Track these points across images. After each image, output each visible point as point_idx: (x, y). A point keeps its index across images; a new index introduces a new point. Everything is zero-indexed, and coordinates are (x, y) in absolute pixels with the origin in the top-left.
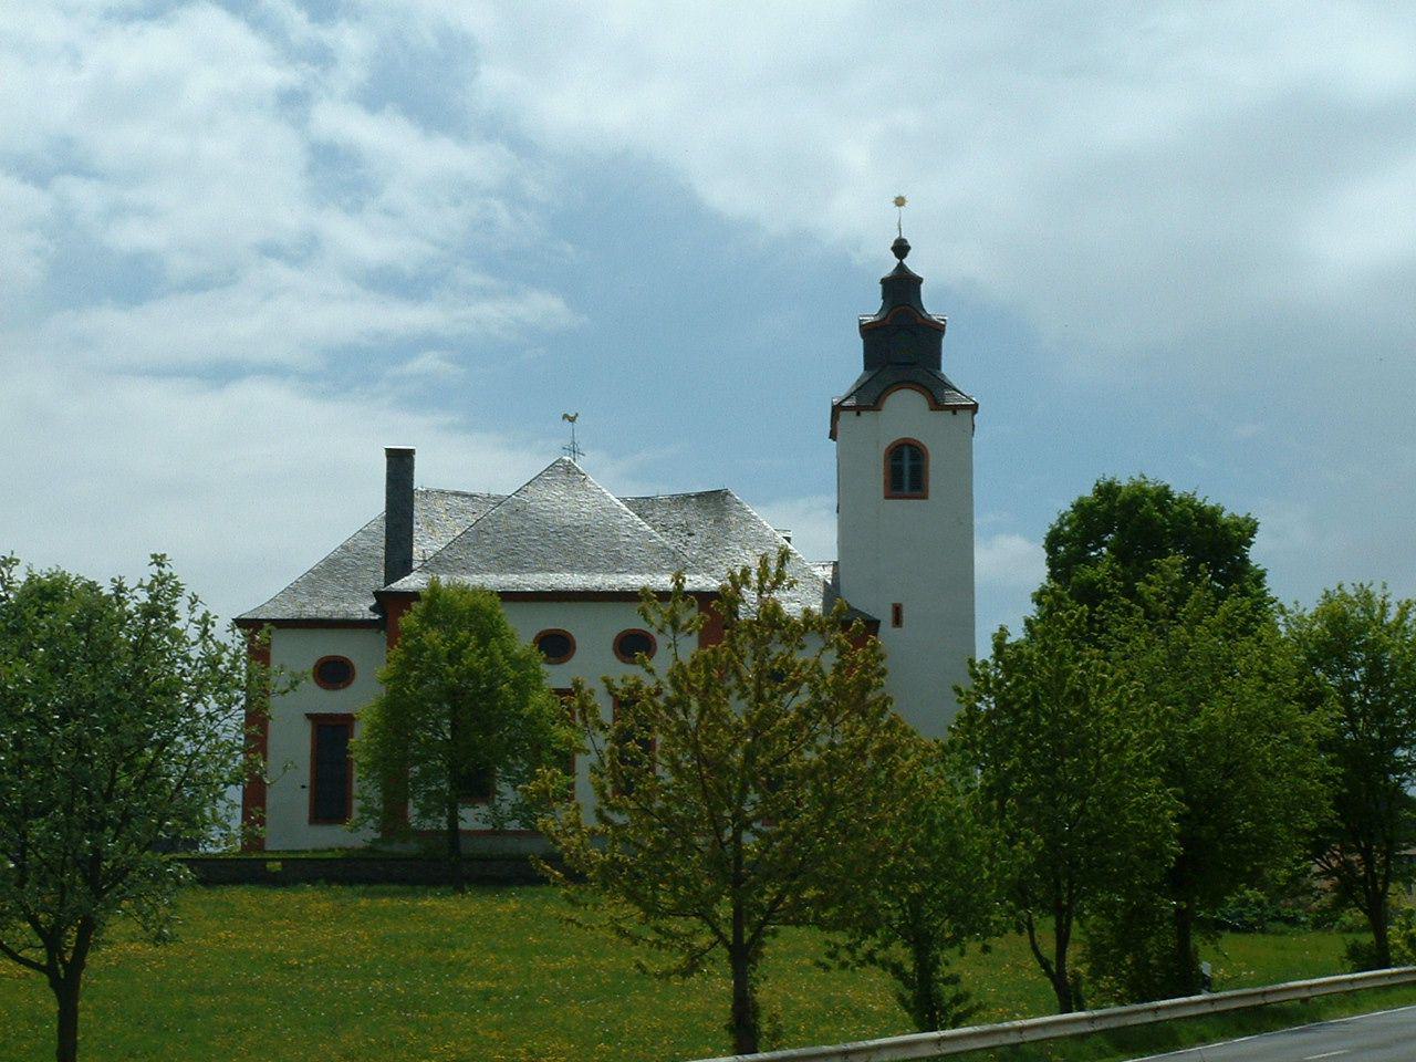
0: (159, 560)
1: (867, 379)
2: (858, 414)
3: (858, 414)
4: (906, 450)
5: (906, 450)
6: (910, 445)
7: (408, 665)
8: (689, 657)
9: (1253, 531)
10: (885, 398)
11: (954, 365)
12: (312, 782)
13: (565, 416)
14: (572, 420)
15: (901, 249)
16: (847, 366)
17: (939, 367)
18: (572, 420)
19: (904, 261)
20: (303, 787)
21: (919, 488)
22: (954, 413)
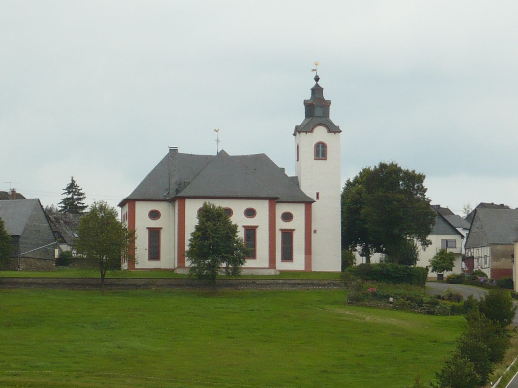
0: (14, 189)
1: (306, 123)
2: (306, 133)
3: (306, 133)
4: (321, 145)
5: (321, 145)
6: (322, 144)
7: (361, 188)
8: (11, 232)
9: (424, 177)
10: (316, 127)
11: (334, 117)
12: (148, 248)
13: (215, 130)
14: (217, 131)
15: (317, 79)
16: (300, 118)
17: (328, 117)
18: (217, 131)
19: (318, 83)
20: (146, 249)
21: (324, 157)
22: (335, 133)
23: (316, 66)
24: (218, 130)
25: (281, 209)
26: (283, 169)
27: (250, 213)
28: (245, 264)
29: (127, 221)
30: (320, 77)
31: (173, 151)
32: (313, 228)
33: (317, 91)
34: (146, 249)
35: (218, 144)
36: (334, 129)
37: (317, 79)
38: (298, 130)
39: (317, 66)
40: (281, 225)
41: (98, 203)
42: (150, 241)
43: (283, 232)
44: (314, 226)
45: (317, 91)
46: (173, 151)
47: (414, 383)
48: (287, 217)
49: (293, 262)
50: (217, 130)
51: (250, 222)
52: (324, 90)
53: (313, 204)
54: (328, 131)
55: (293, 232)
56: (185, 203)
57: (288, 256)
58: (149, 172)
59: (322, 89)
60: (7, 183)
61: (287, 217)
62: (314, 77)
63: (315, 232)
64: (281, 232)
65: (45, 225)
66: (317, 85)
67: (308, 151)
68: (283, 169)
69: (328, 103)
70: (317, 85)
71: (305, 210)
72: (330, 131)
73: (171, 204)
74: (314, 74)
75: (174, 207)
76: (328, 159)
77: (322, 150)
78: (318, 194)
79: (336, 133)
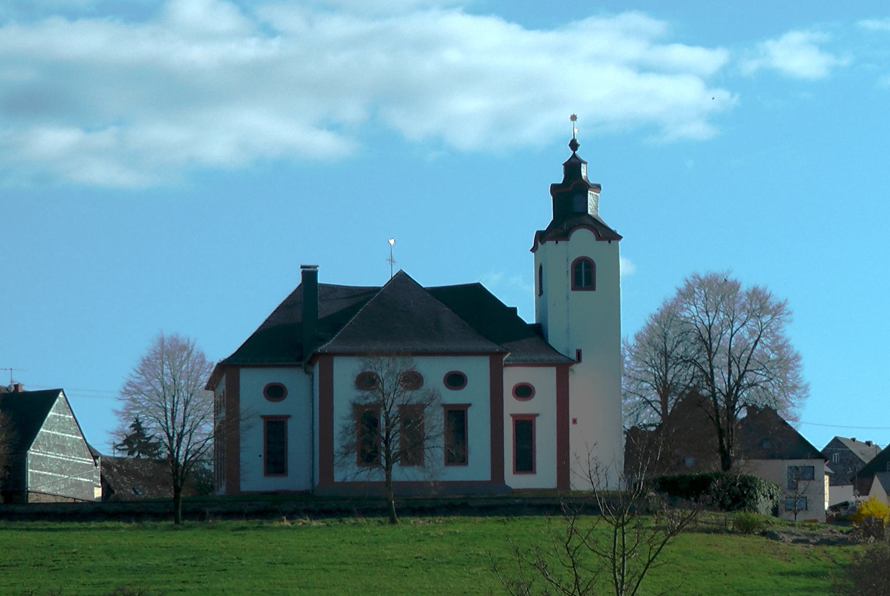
3: (610, 242)
16: (545, 217)
20: (260, 456)
25: (513, 377)
26: (514, 310)
27: (456, 380)
29: (224, 481)
32: (572, 416)
33: (573, 167)
34: (260, 456)
36: (608, 236)
38: (541, 237)
40: (512, 406)
42: (268, 442)
43: (516, 421)
44: (573, 412)
45: (573, 167)
47: (785, 310)
48: (524, 391)
49: (535, 473)
51: (453, 397)
55: (535, 420)
57: (526, 463)
60: (6, 369)
61: (524, 391)
63: (575, 421)
64: (513, 418)
65: (74, 437)
66: (574, 155)
67: (561, 277)
68: (514, 310)
70: (574, 155)
72: (599, 238)
75: (312, 375)
78: (579, 353)
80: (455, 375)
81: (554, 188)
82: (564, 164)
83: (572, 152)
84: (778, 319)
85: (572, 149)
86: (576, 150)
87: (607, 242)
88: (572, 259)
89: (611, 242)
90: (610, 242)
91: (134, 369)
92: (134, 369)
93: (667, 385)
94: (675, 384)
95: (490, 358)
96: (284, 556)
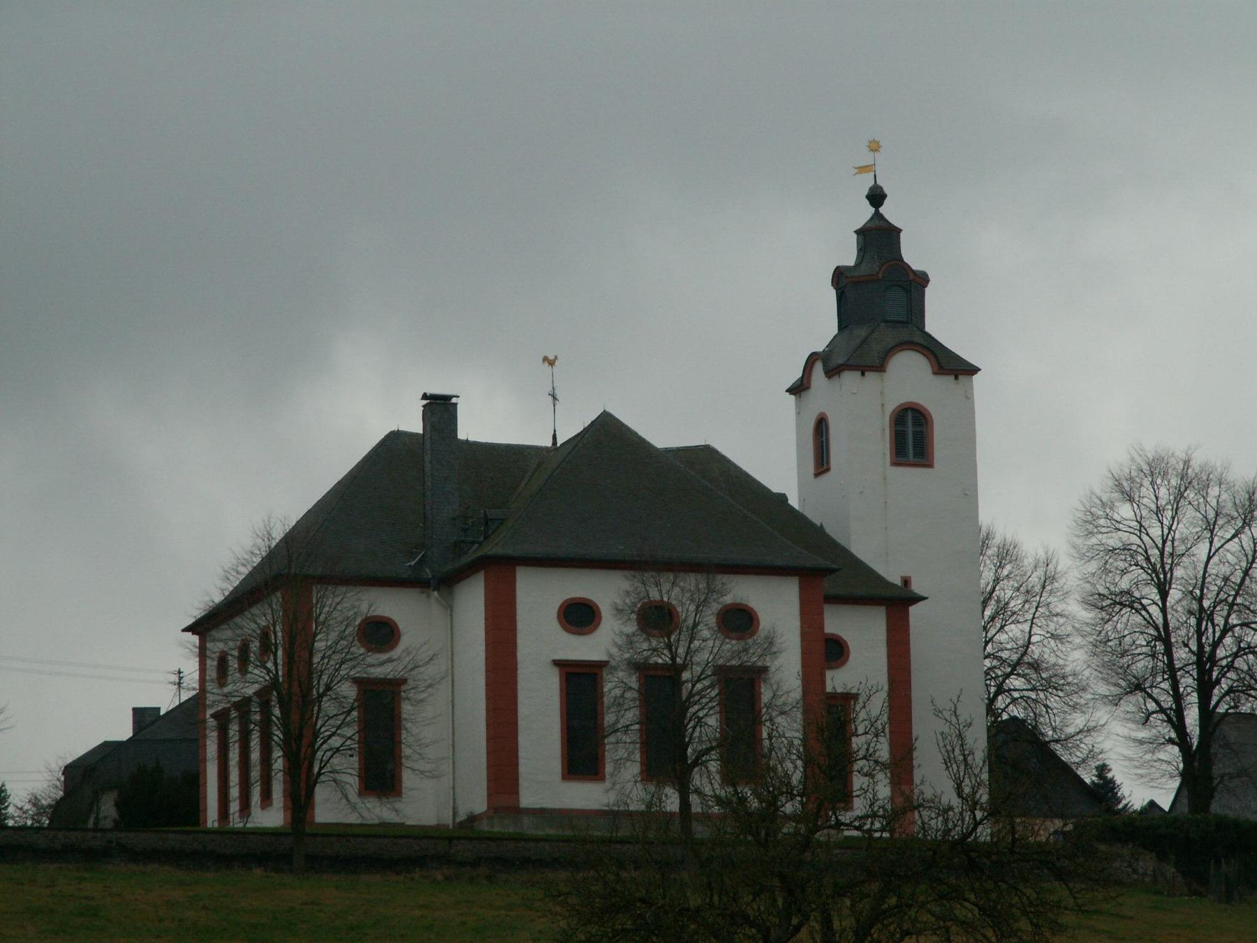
3: (863, 374)
13: (545, 359)
15: (876, 197)
19: (882, 210)
22: (956, 378)
23: (871, 153)
24: (556, 357)
28: (1032, 546)
30: (886, 190)
31: (901, 230)
35: (554, 405)
37: (876, 197)
39: (877, 154)
41: (237, 566)
46: (901, 230)
50: (551, 357)
52: (902, 235)
53: (913, 610)
54: (933, 367)
56: (515, 576)
58: (310, 506)
59: (898, 231)
62: (866, 192)
66: (878, 216)
69: (922, 280)
70: (878, 216)
71: (889, 631)
73: (439, 593)
74: (866, 183)
76: (935, 465)
77: (914, 433)
79: (961, 377)
80: (578, 604)
81: (840, 277)
82: (858, 232)
83: (872, 210)
84: (344, 707)
85: (872, 204)
86: (881, 204)
87: (953, 377)
88: (890, 408)
89: (866, 373)
90: (863, 374)
91: (1082, 502)
92: (1082, 502)
93: (35, 825)
94: (764, 805)
95: (800, 582)
96: (935, 797)
